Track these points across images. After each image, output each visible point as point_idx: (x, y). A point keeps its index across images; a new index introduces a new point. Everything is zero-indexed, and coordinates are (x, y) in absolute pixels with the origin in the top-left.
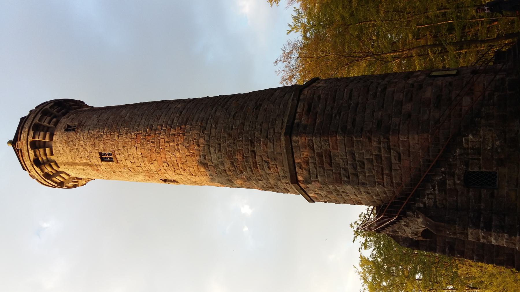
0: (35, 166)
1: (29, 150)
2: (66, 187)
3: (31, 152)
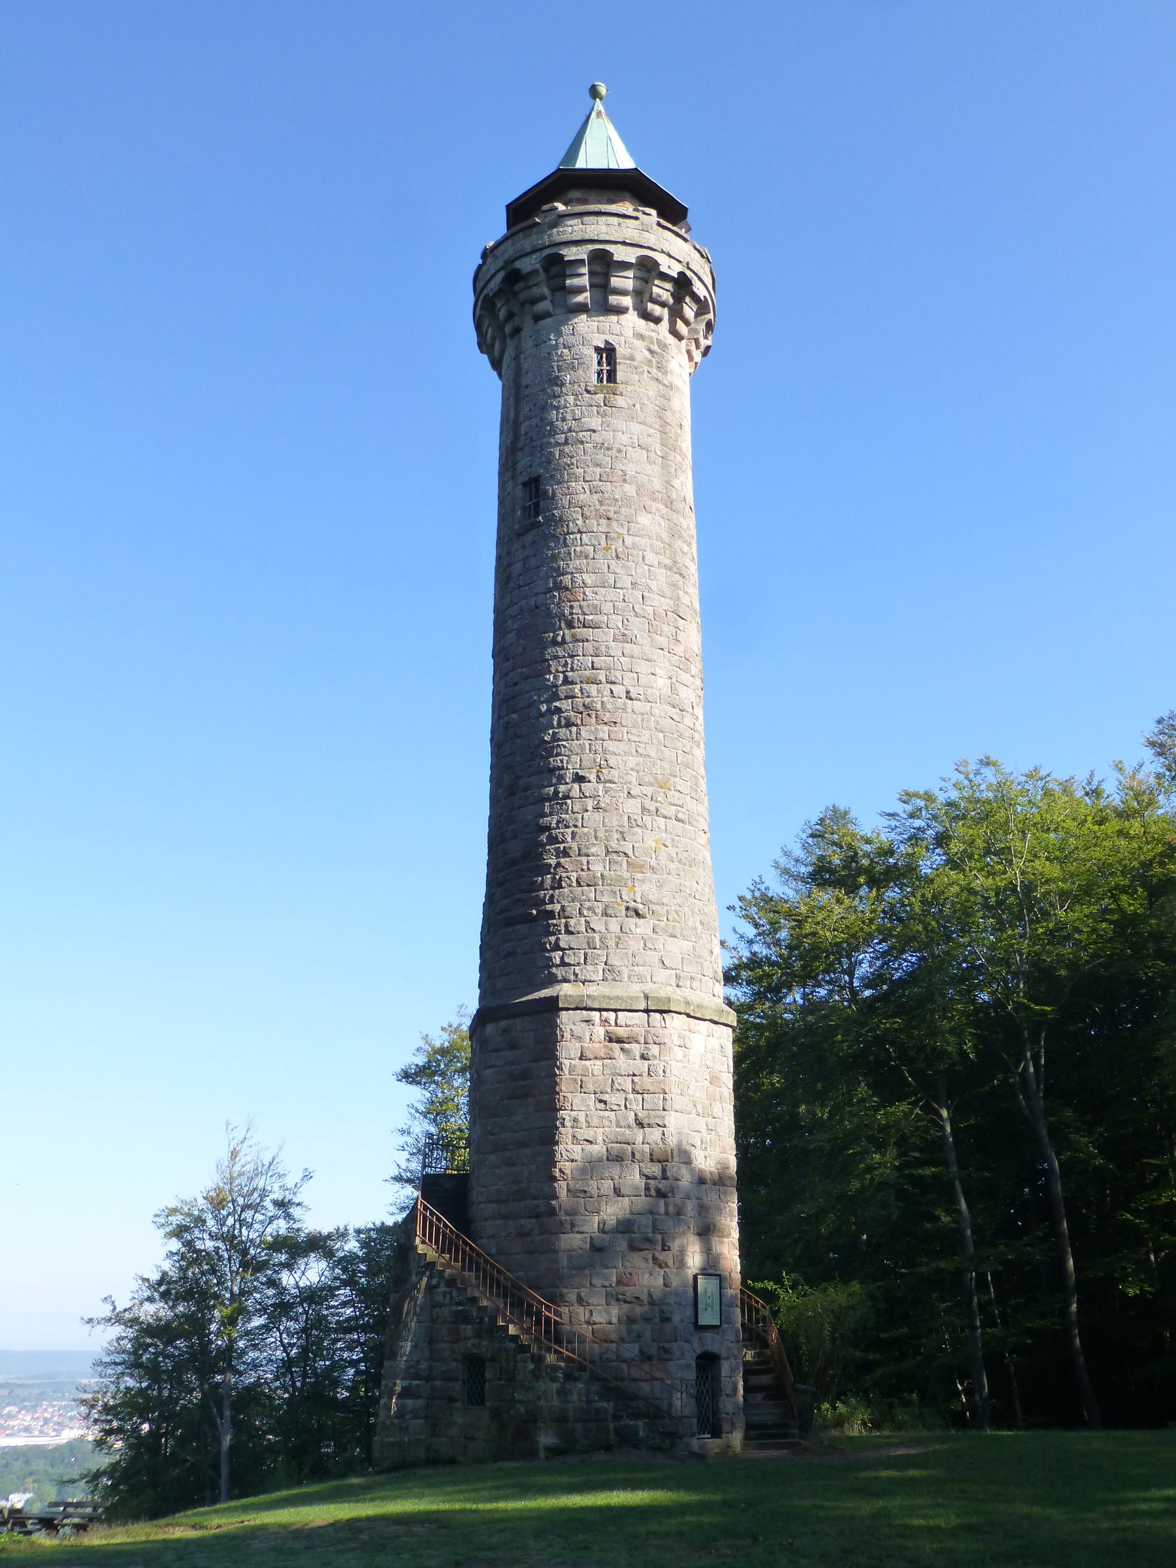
0: (502, 274)
1: (538, 254)
2: (480, 316)
3: (533, 262)
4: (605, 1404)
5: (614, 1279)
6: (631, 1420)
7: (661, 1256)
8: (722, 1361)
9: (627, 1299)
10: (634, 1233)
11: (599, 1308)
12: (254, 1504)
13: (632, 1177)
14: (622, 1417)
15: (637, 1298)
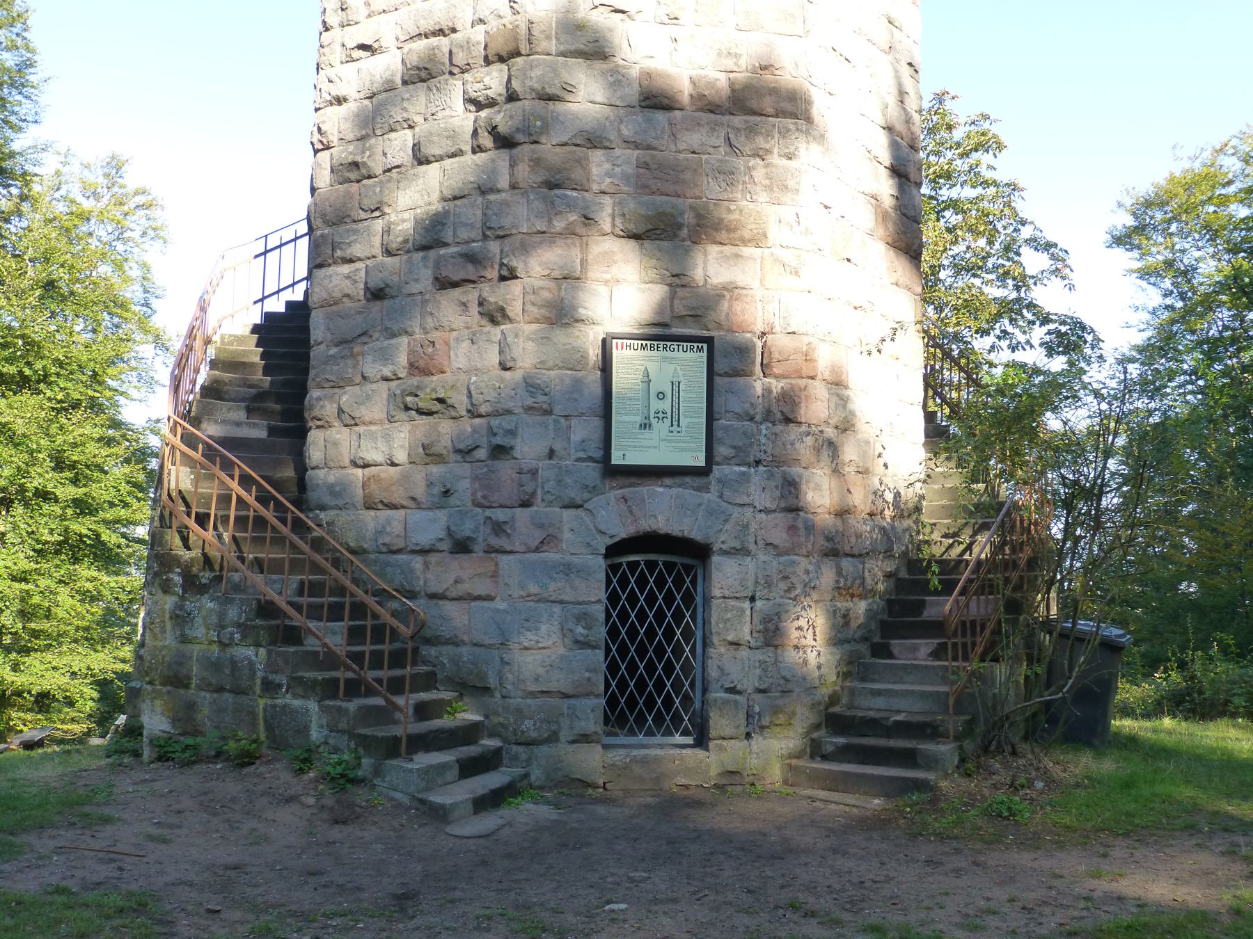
4: (250, 652)
5: (403, 359)
6: (295, 696)
7: (495, 294)
8: (715, 559)
9: (421, 405)
10: (446, 245)
11: (373, 428)
12: (428, 749)
13: (448, 112)
14: (280, 686)
15: (441, 401)
